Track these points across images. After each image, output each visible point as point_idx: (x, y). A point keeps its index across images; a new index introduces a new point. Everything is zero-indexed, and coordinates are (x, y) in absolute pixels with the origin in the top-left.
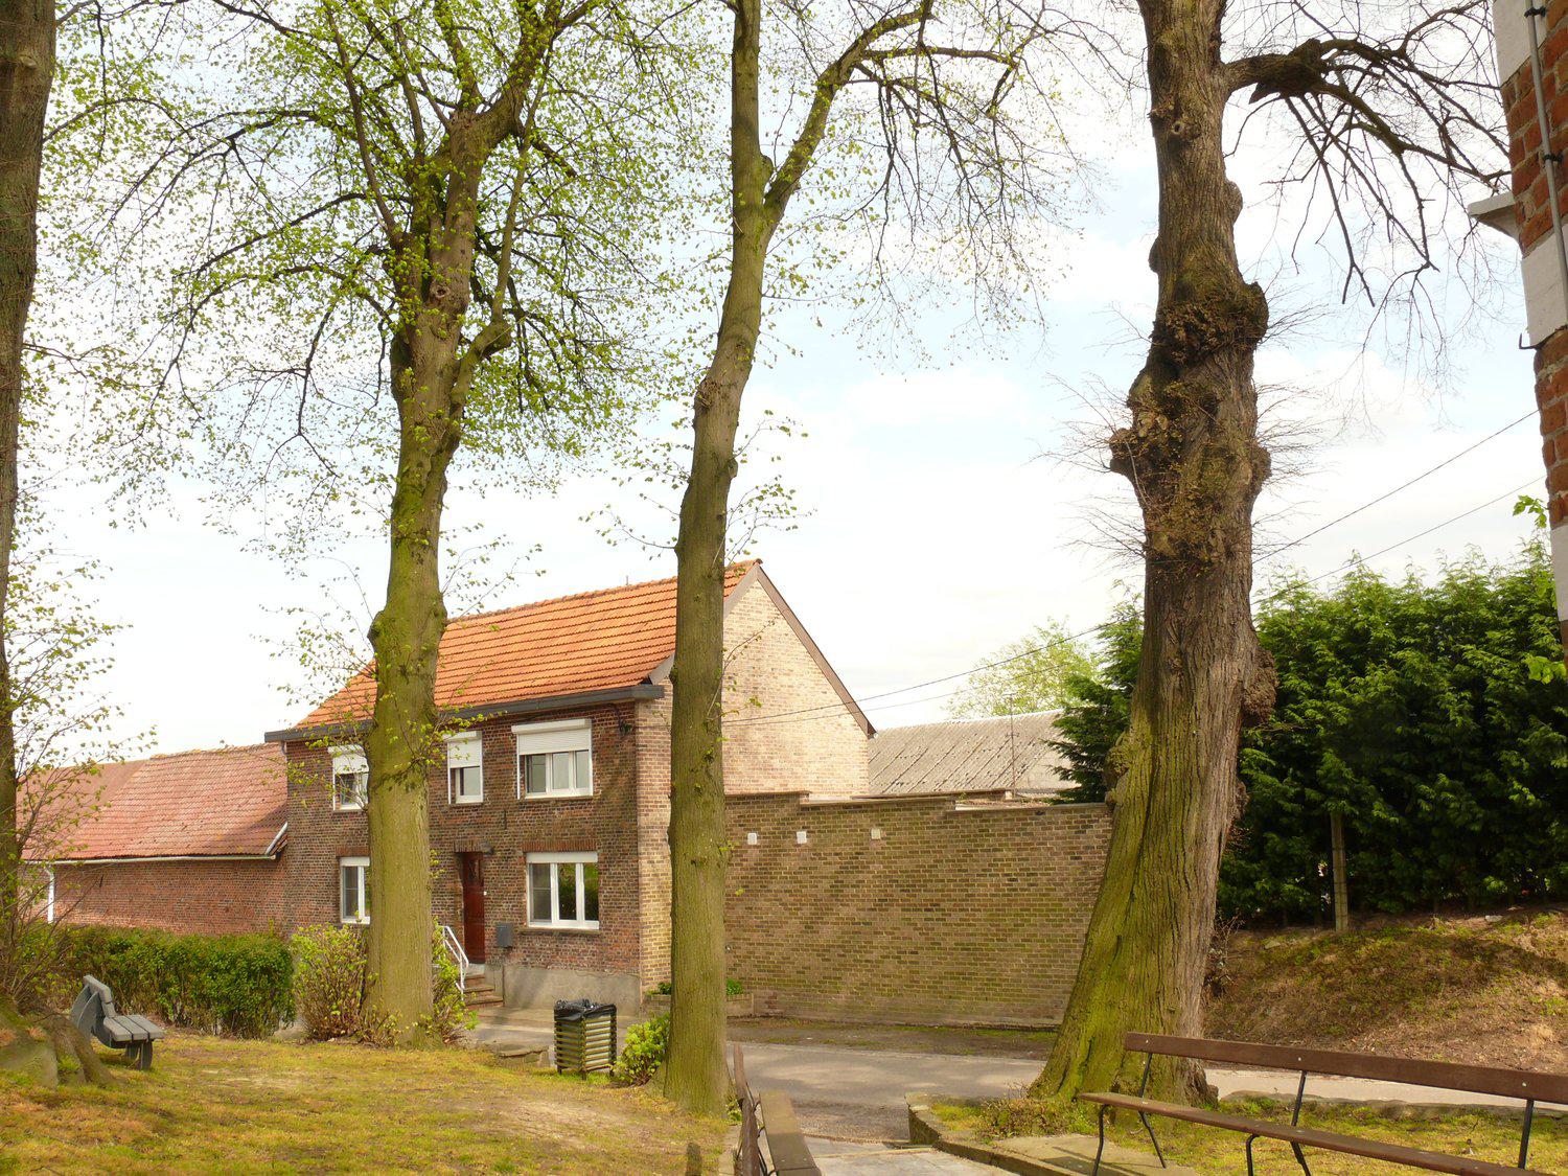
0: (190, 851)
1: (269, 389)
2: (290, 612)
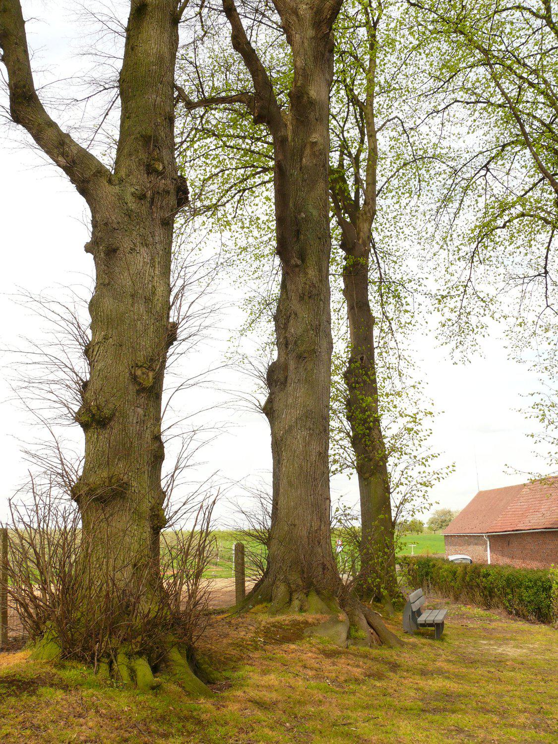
0: (544, 527)
1: (530, 287)
2: (532, 395)
